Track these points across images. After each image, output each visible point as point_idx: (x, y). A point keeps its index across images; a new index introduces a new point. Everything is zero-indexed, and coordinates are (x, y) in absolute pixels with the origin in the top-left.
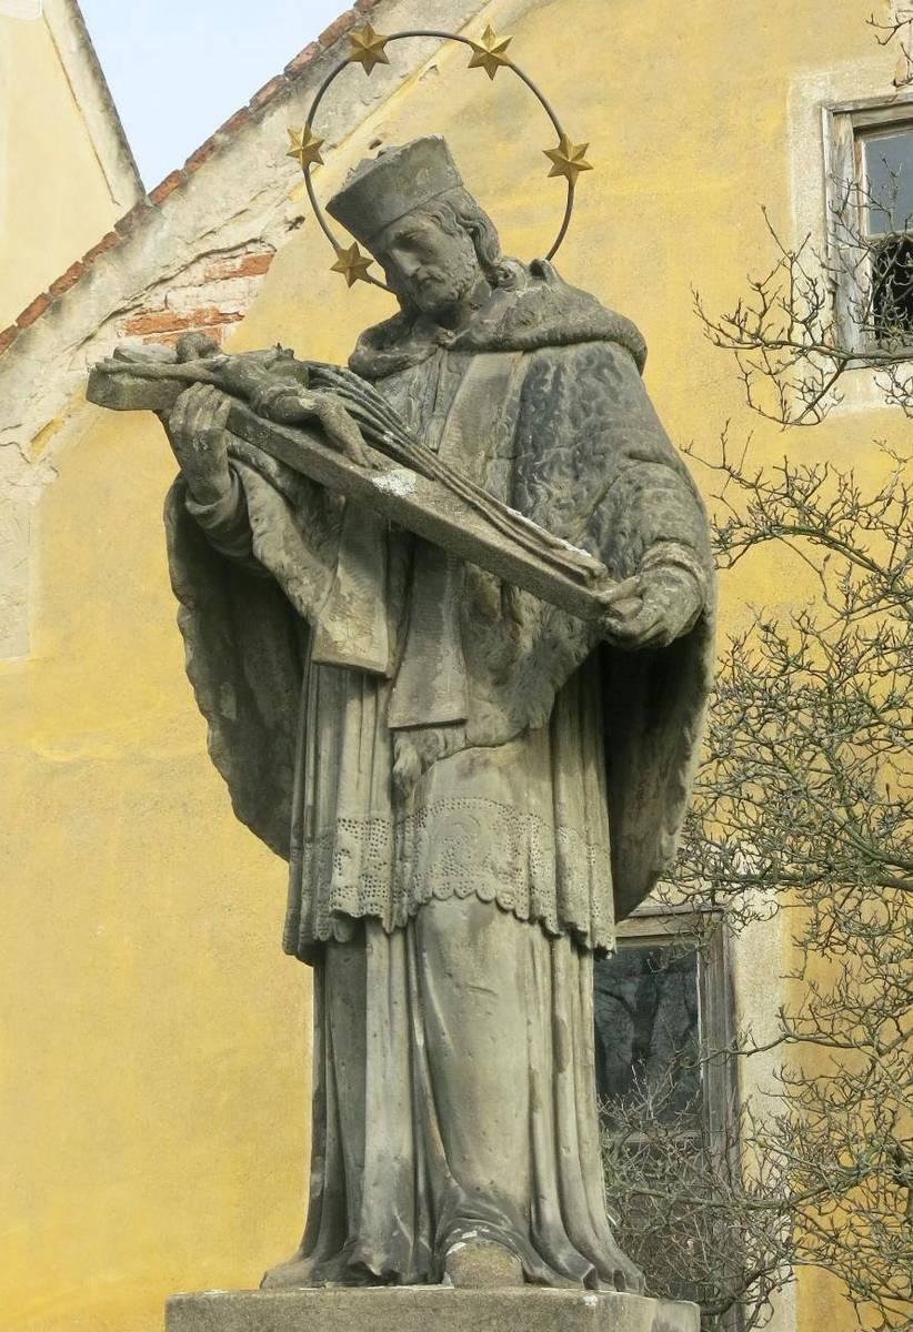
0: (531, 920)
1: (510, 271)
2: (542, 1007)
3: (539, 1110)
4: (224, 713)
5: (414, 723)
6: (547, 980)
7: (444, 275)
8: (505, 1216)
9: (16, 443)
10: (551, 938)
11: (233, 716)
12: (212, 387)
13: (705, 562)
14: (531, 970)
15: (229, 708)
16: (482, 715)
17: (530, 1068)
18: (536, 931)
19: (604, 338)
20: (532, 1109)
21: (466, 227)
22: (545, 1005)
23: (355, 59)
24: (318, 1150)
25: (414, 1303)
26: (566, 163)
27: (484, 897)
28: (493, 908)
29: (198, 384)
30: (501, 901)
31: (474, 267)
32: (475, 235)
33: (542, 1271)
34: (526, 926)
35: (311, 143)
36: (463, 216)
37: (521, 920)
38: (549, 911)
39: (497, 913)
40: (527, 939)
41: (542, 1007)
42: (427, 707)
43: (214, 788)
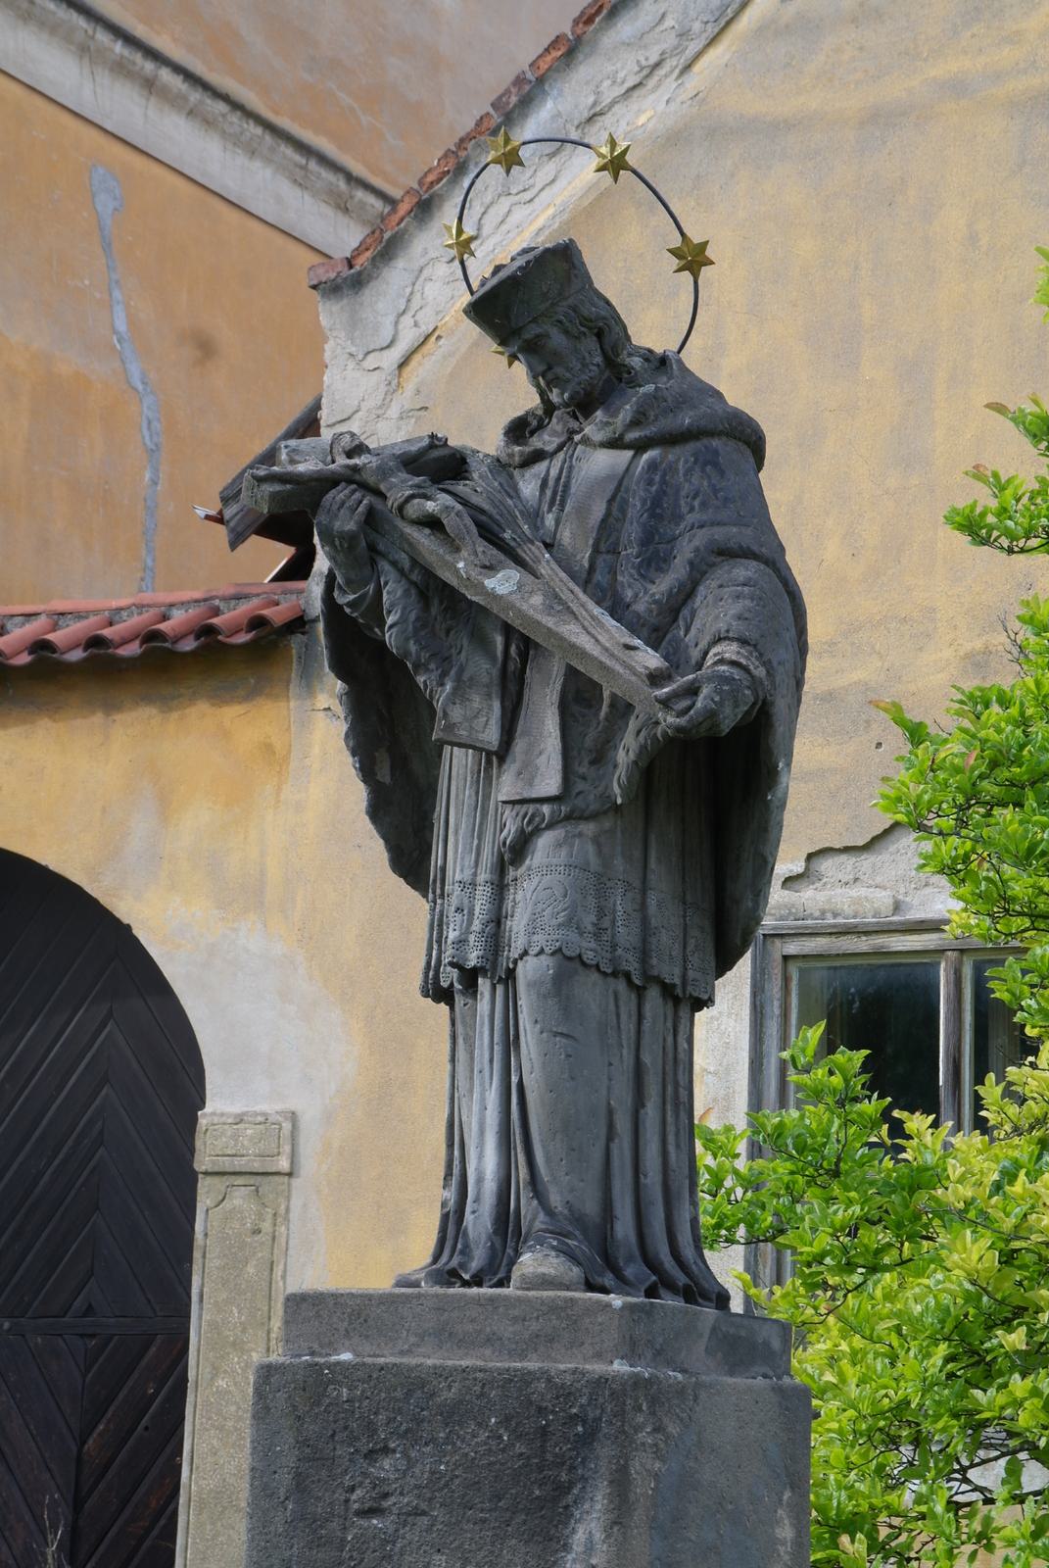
0: (615, 974)
1: (633, 368)
2: (625, 1051)
3: (616, 1141)
4: (379, 778)
5: (518, 798)
6: (632, 1027)
7: (568, 375)
8: (577, 1233)
9: (388, 347)
10: (640, 991)
11: (387, 780)
12: (354, 486)
13: (765, 659)
14: (614, 1018)
15: (384, 775)
16: (577, 791)
17: (609, 1104)
18: (621, 986)
19: (711, 434)
20: (610, 1138)
21: (590, 328)
22: (629, 1048)
23: (496, 161)
24: (449, 1174)
25: (492, 1299)
26: (693, 259)
27: (568, 953)
28: (577, 965)
29: (343, 484)
30: (585, 958)
31: (598, 365)
32: (599, 335)
33: (608, 1280)
34: (611, 980)
35: (464, 237)
36: (585, 319)
37: (605, 974)
38: (632, 965)
39: (580, 969)
40: (611, 991)
41: (625, 1051)
42: (530, 783)
43: (376, 849)
